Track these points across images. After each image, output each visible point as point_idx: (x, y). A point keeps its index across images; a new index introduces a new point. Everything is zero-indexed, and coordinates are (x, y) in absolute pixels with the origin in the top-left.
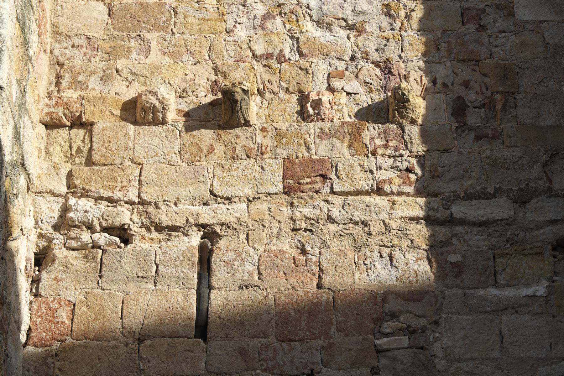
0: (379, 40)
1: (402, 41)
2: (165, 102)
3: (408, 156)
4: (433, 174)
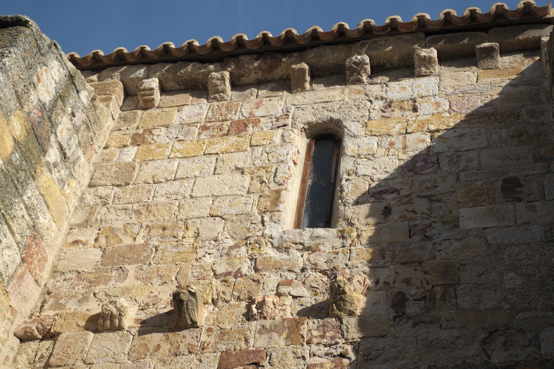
0: (330, 255)
1: (350, 253)
2: (122, 309)
3: (343, 344)
4: (366, 357)
